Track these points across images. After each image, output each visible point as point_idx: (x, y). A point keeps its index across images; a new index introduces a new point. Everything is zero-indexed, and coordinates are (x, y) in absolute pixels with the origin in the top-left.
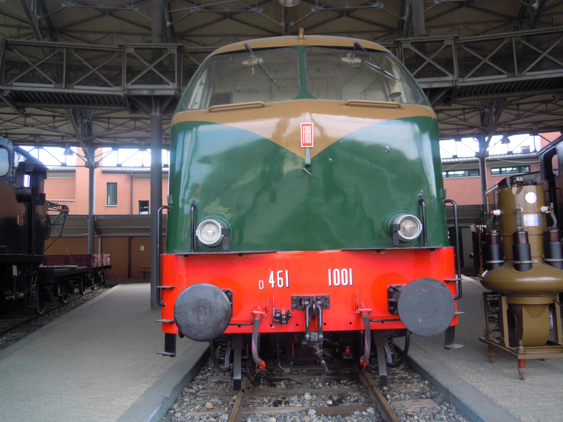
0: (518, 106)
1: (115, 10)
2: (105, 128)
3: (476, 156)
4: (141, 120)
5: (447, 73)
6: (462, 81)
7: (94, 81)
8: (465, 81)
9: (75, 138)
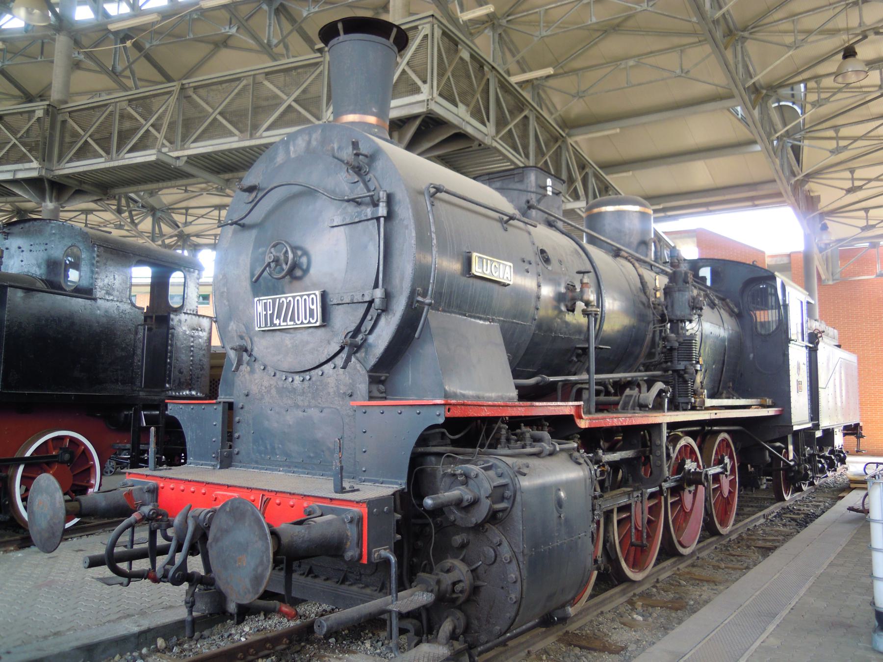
0: (837, 132)
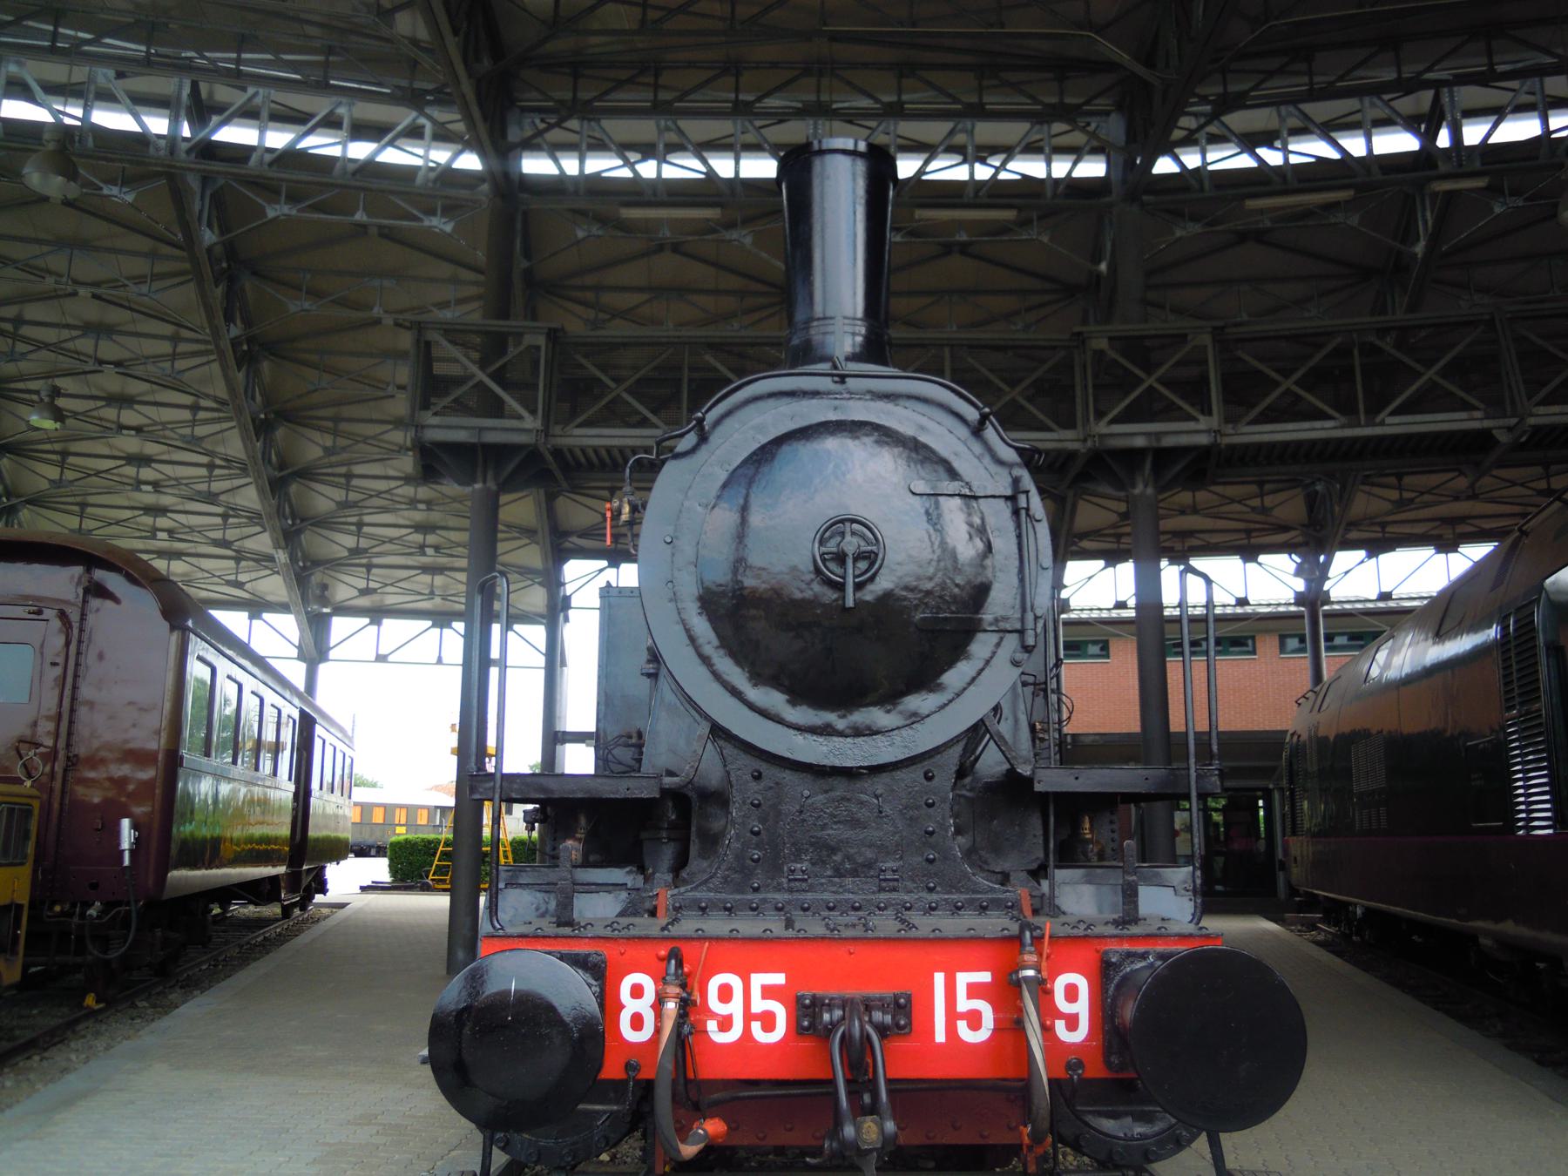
3: (1297, 603)
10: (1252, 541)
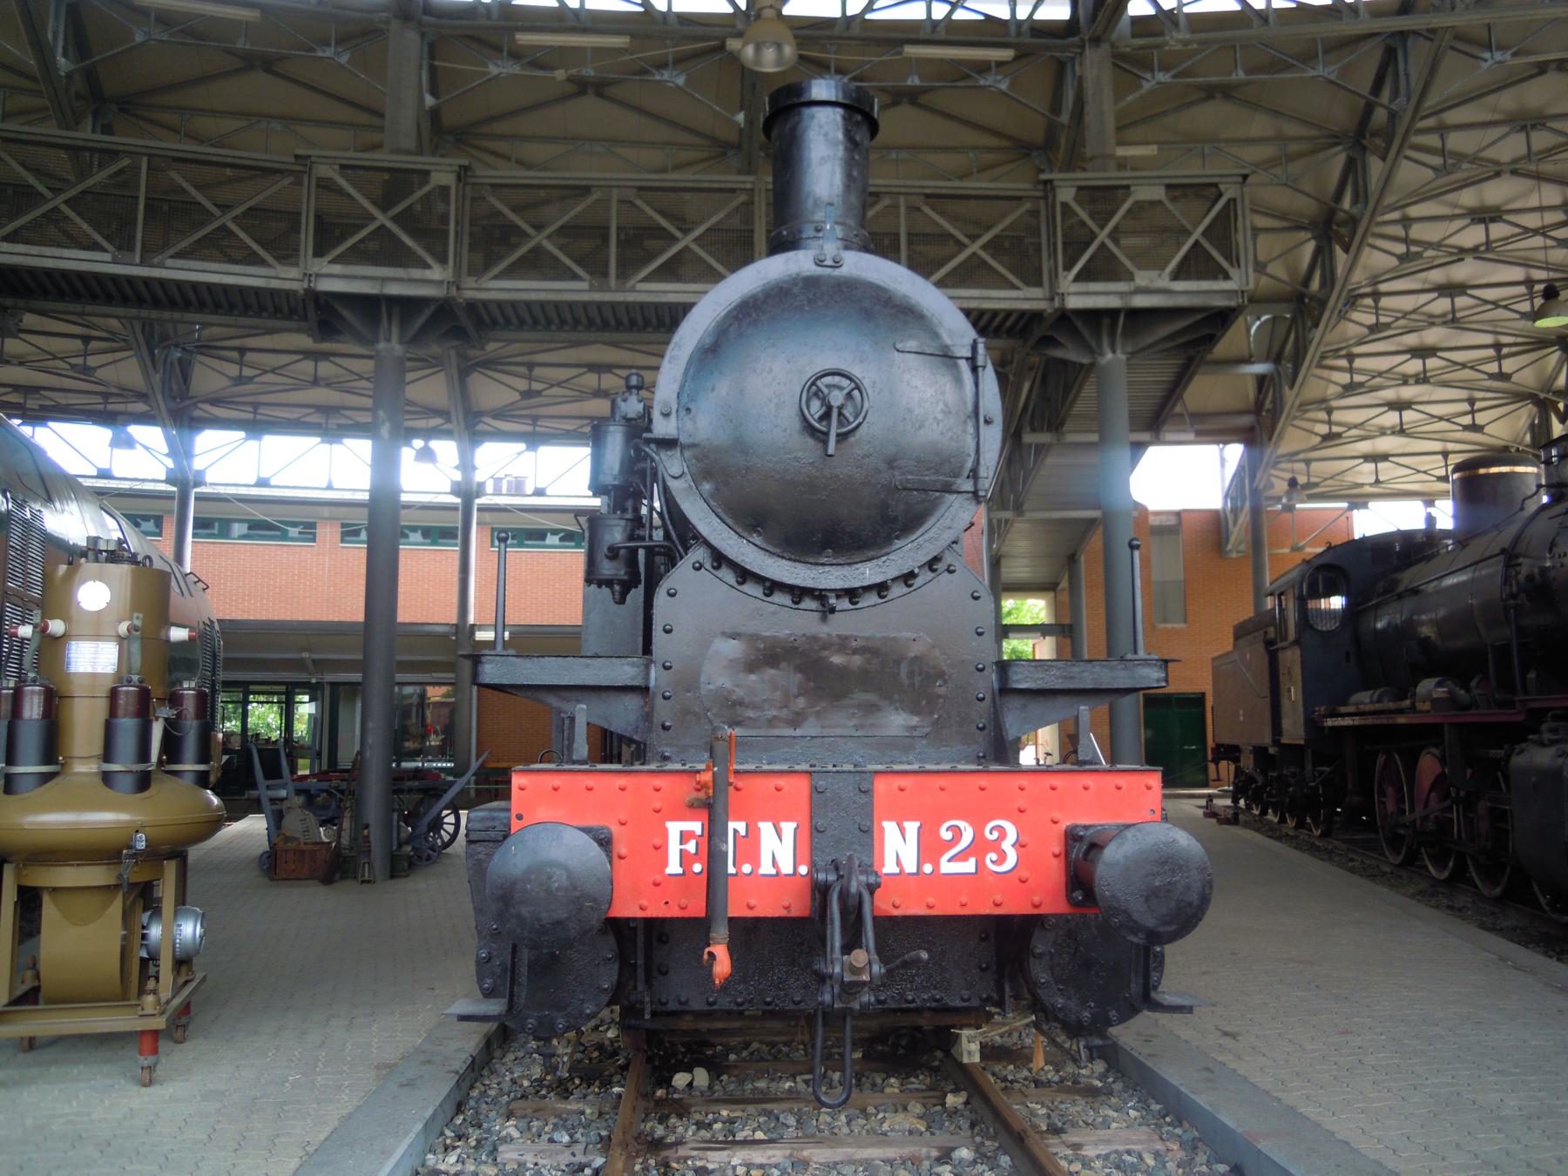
1: (283, 58)
2: (231, 378)
3: (168, 481)
4: (615, 371)
5: (429, 260)
6: (474, 285)
7: (218, 246)
8: (484, 286)
9: (145, 402)
10: (110, 407)
